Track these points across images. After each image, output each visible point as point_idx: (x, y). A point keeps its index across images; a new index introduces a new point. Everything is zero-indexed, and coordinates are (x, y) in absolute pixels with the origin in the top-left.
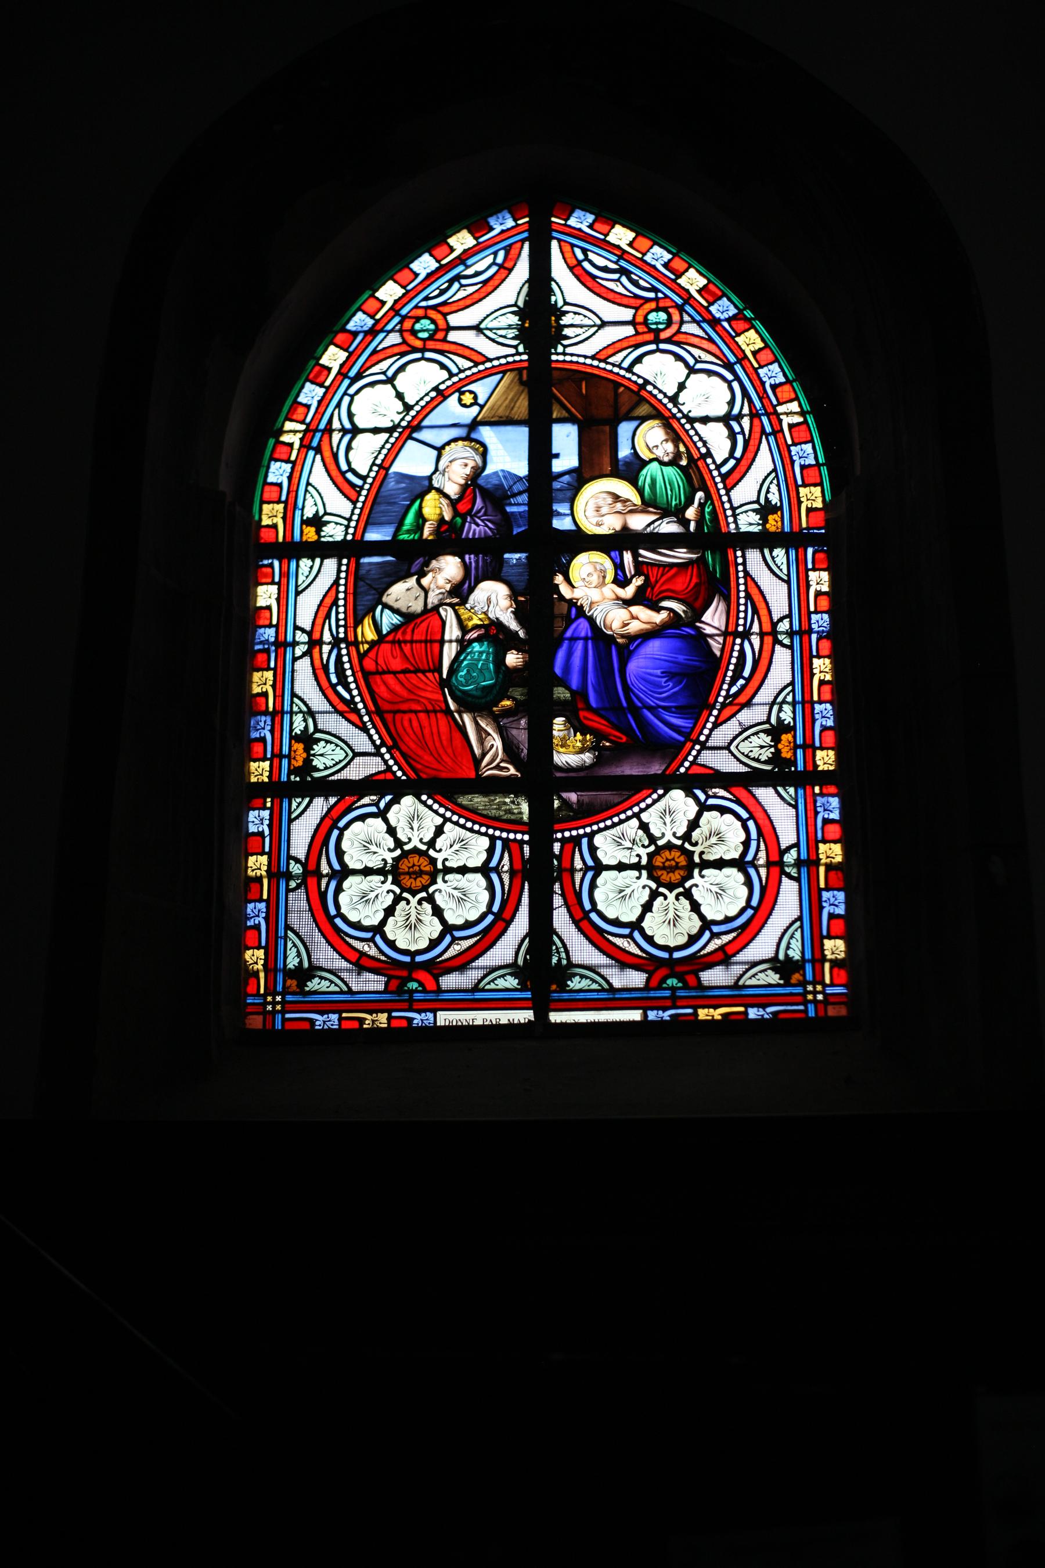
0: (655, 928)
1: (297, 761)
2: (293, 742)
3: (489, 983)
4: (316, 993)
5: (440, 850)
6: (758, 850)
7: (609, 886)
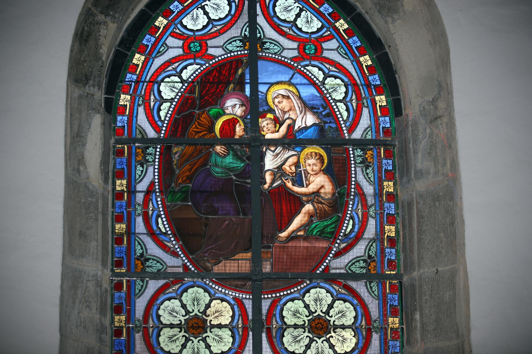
0: (342, 348)
1: (138, 269)
2: (136, 260)
3: (138, 242)
4: (136, 169)
5: (307, 337)
6: (238, 320)
7: (349, 318)
